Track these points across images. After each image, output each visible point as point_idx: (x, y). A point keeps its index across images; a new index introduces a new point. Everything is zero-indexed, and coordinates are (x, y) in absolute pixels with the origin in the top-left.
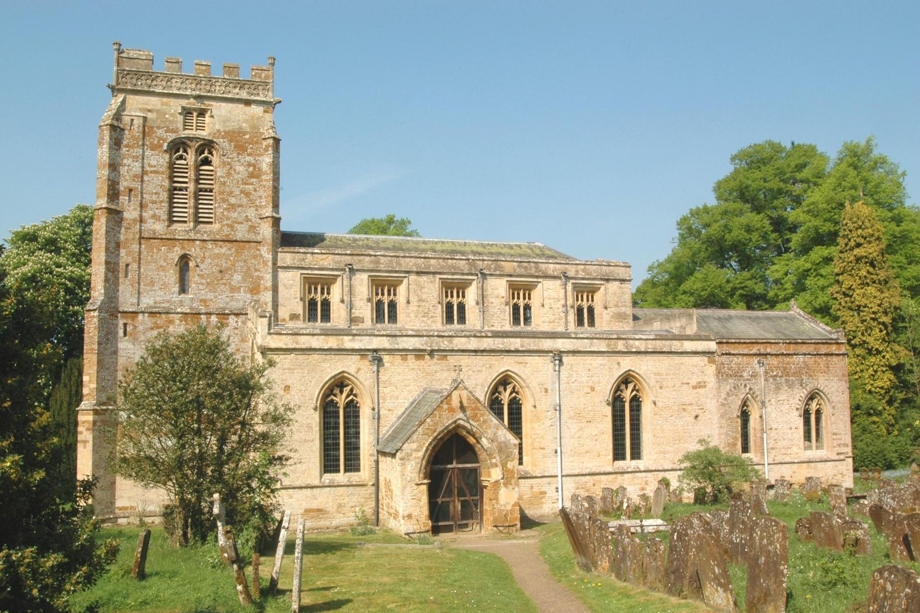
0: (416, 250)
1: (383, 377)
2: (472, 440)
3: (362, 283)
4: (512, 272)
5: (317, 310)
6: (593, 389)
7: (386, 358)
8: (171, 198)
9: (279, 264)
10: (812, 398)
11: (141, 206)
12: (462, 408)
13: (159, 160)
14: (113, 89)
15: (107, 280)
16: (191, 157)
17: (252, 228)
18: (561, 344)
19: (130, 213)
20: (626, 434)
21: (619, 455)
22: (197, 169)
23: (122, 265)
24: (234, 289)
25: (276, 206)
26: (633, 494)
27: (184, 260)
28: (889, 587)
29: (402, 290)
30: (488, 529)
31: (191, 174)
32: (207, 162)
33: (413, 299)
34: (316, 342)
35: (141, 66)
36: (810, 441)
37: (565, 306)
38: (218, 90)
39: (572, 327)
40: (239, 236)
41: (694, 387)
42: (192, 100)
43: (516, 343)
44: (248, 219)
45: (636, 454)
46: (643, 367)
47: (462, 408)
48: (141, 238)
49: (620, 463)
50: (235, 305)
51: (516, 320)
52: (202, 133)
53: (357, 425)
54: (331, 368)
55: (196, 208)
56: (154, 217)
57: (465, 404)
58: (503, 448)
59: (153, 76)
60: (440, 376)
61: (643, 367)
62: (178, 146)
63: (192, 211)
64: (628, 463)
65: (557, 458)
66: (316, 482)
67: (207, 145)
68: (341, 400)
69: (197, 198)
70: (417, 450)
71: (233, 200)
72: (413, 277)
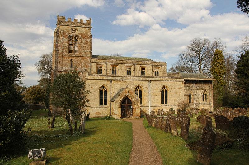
0: (121, 59)
1: (112, 85)
2: (130, 99)
3: (109, 65)
4: (141, 64)
5: (100, 71)
6: (157, 89)
7: (113, 81)
8: (69, 48)
9: (92, 61)
10: (204, 92)
11: (63, 49)
12: (128, 92)
13: (66, 40)
14: (57, 24)
15: (55, 65)
16: (73, 39)
17: (86, 54)
18: (150, 79)
19: (60, 51)
20: (164, 97)
21: (162, 103)
22: (74, 41)
23: (59, 62)
24: (82, 67)
25: (91, 49)
26: (165, 111)
27: (72, 60)
28: (207, 132)
29: (117, 67)
30: (133, 118)
31: (73, 43)
32: (76, 40)
33: (120, 69)
34: (98, 78)
35: (63, 20)
36: (204, 100)
37: (152, 71)
38: (79, 25)
39: (154, 76)
40: (83, 56)
41: (179, 89)
42: (73, 27)
43: (141, 79)
44: (85, 52)
45: (166, 103)
46: (168, 84)
47: (128, 92)
48: (63, 56)
49: (163, 104)
50: (82, 70)
51: (142, 74)
52: (76, 34)
53: (107, 95)
54: (101, 83)
55: (74, 50)
56: (65, 51)
57: (129, 91)
58: (137, 101)
59: (65, 22)
60: (123, 85)
61: (168, 84)
62: (70, 37)
63: (73, 50)
64: (164, 104)
65: (151, 103)
66: (98, 107)
67: (76, 37)
68: (103, 90)
69: (74, 48)
70: (119, 100)
71: (82, 48)
72: (120, 65)
